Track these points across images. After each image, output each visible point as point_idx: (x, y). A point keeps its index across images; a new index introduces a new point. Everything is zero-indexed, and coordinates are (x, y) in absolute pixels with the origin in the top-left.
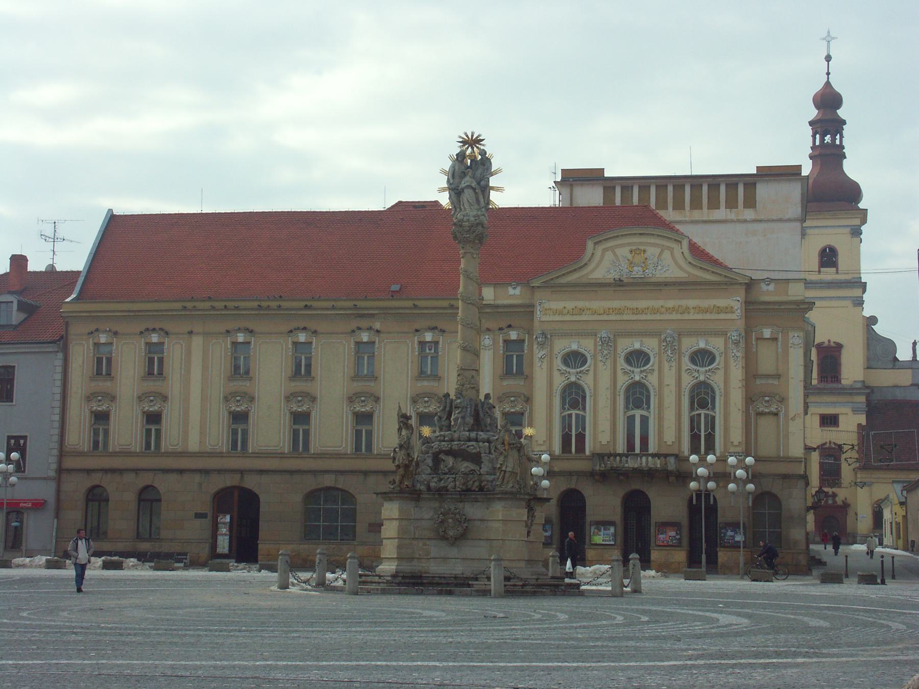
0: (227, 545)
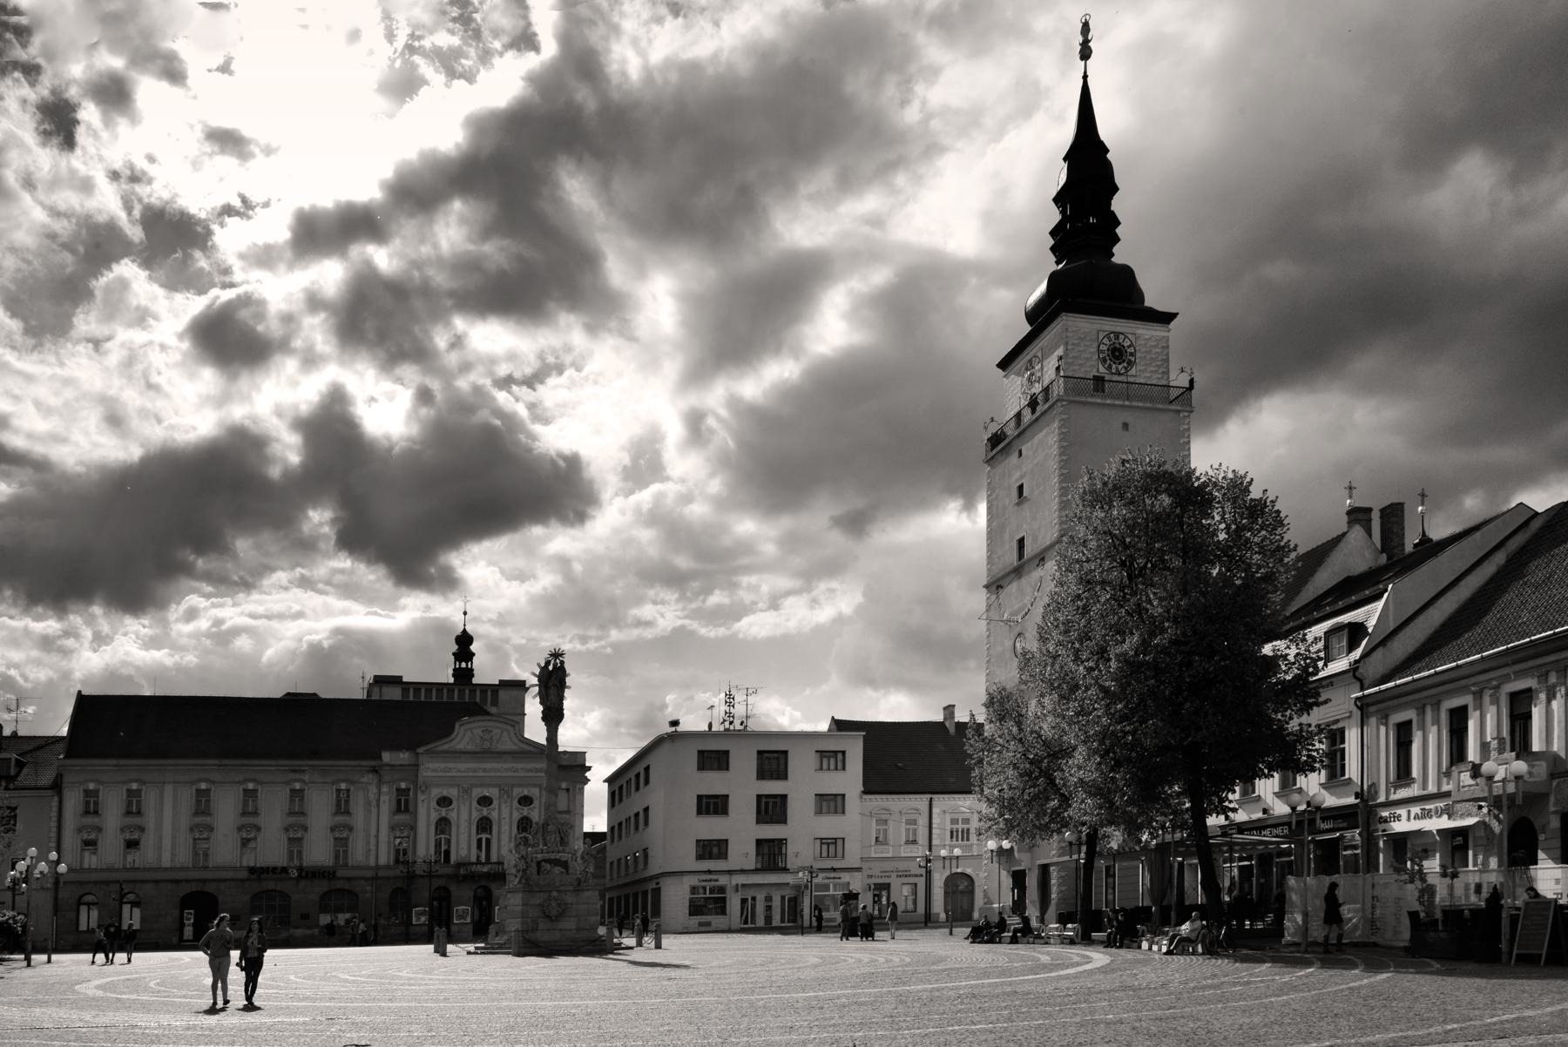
0: (191, 933)
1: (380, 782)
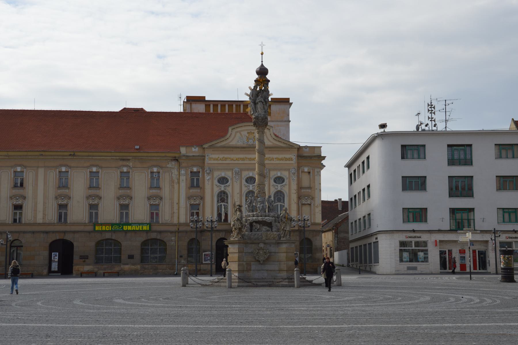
0: (57, 267)
1: (180, 167)
